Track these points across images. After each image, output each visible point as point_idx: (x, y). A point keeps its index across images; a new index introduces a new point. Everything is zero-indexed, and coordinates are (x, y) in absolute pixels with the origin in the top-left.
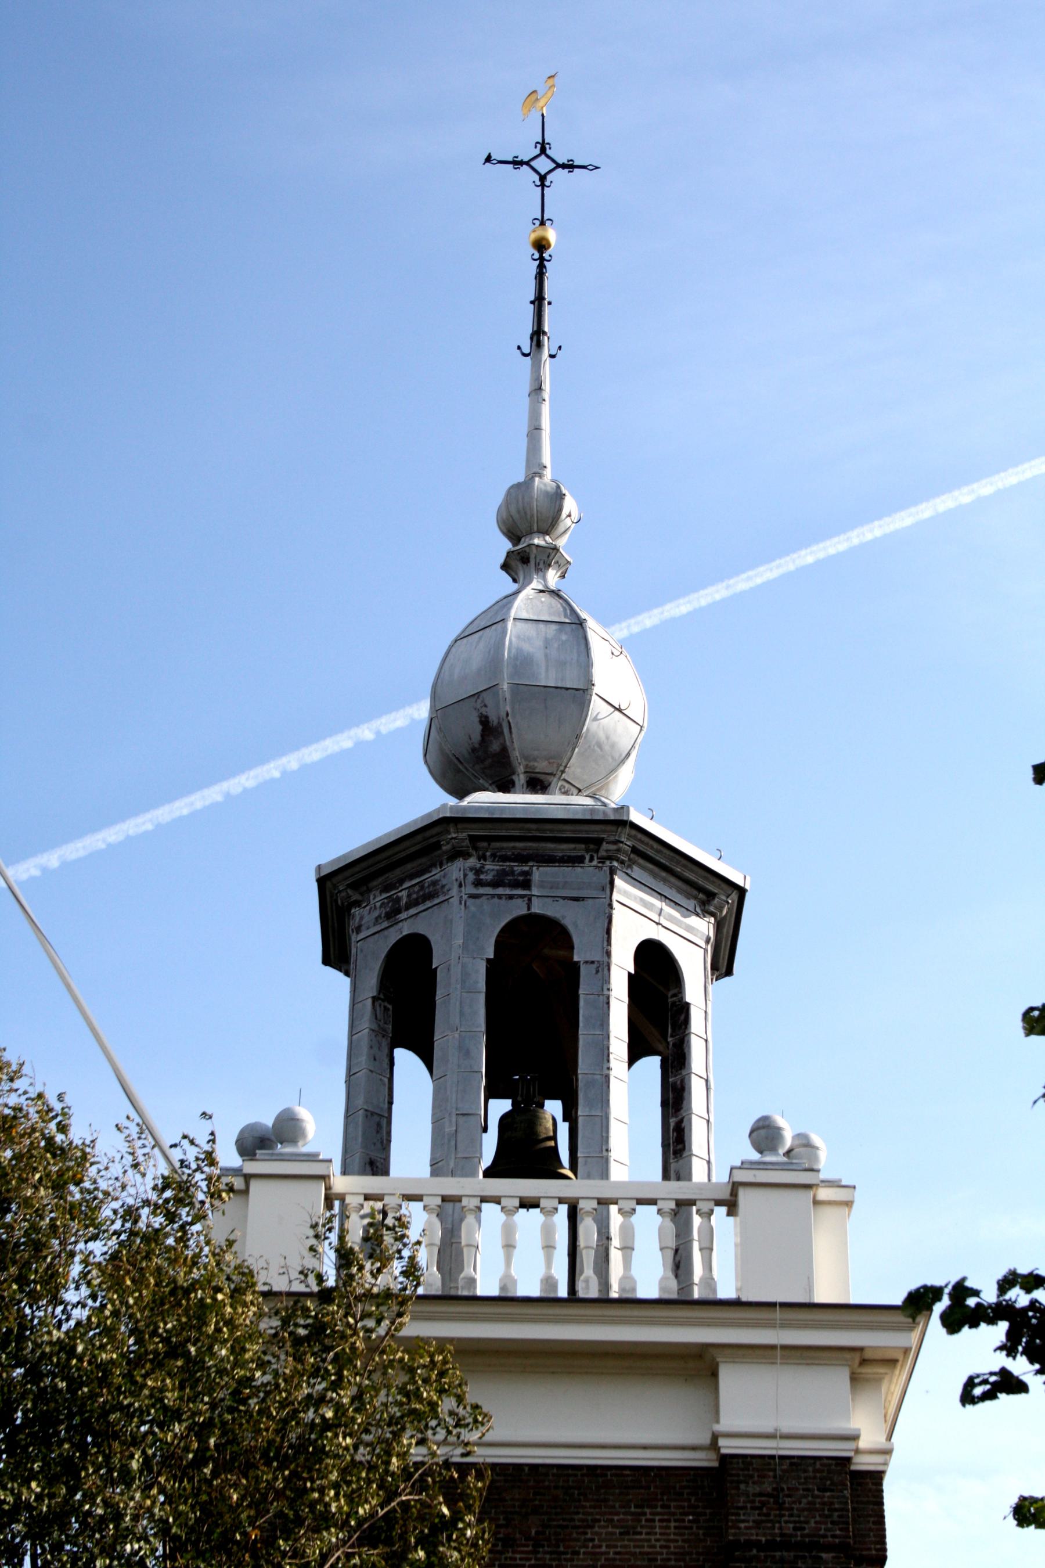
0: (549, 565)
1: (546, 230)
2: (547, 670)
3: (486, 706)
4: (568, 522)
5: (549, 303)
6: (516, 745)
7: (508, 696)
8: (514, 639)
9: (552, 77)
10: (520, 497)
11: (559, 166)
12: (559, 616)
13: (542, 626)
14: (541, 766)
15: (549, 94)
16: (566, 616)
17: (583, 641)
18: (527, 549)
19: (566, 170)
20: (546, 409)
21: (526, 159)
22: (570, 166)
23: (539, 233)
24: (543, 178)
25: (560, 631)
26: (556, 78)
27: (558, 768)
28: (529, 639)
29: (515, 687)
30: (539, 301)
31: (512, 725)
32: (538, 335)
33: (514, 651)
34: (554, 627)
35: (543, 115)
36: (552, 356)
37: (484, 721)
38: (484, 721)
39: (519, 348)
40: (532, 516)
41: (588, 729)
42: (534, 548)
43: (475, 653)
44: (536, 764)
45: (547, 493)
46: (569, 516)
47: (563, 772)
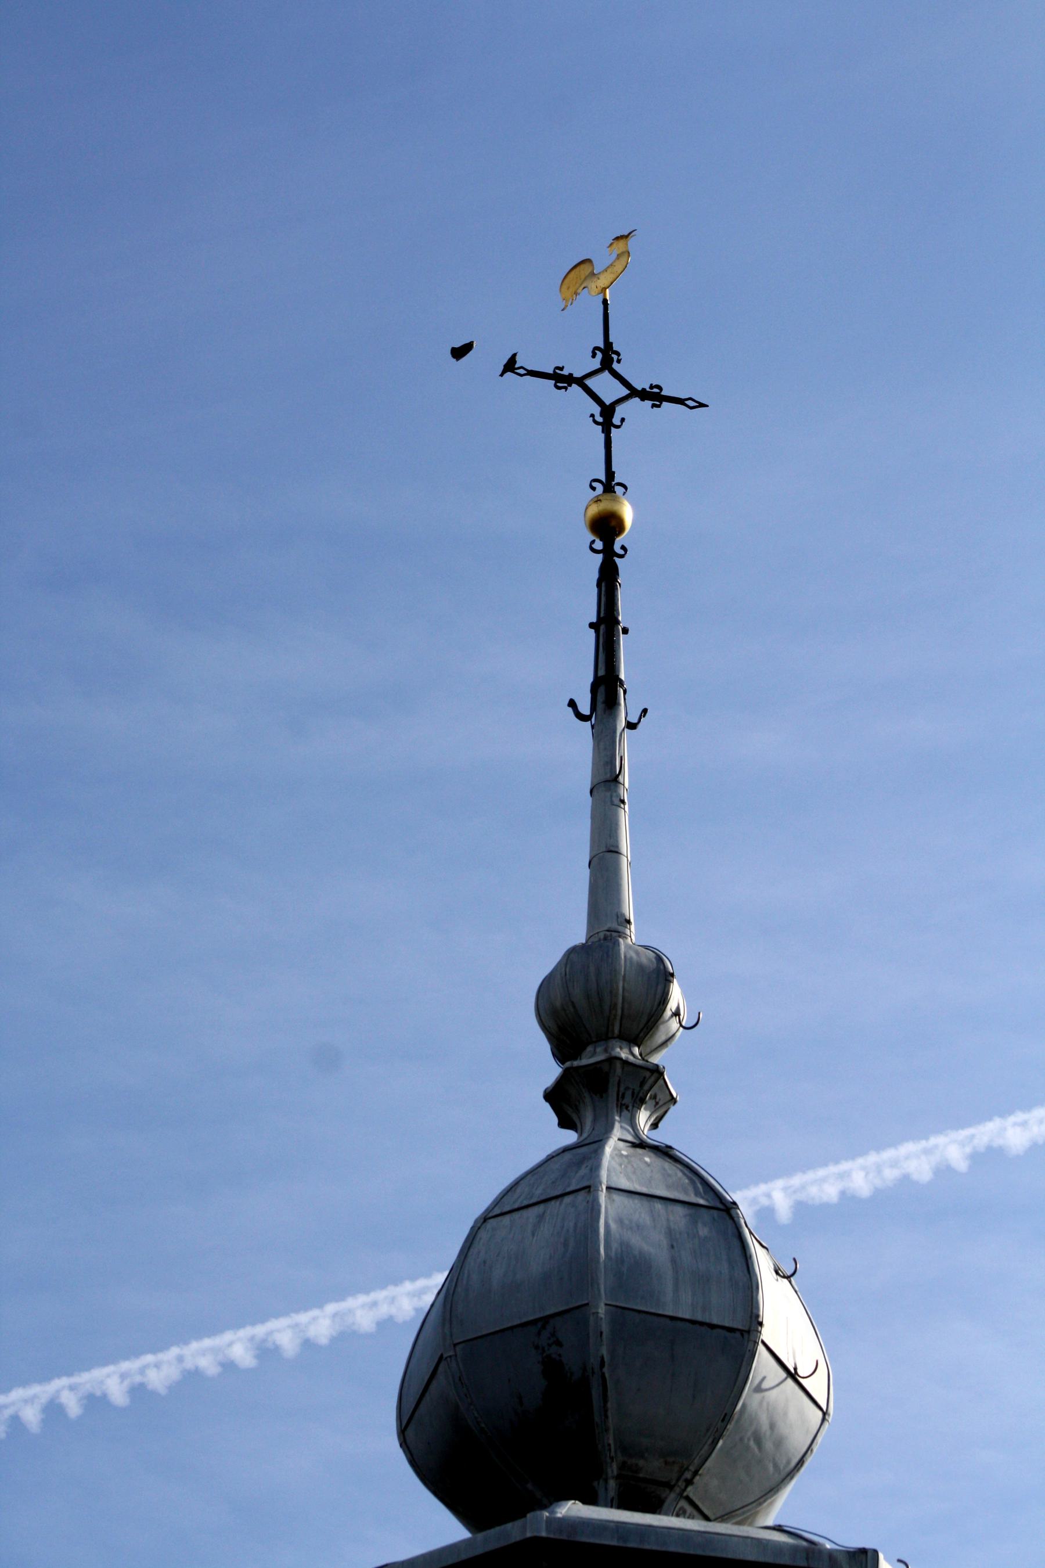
0: (642, 1101)
1: (616, 500)
2: (676, 1289)
3: (559, 1344)
4: (674, 1024)
5: (625, 631)
6: (611, 1423)
7: (605, 1328)
8: (613, 1226)
9: (627, 237)
10: (592, 969)
11: (634, 393)
12: (686, 1193)
13: (658, 1206)
14: (652, 1467)
15: (619, 267)
16: (697, 1193)
17: (736, 1242)
18: (606, 1067)
19: (648, 403)
20: (624, 818)
21: (577, 374)
22: (655, 396)
23: (605, 506)
24: (608, 411)
25: (694, 1221)
26: (631, 241)
27: (681, 1473)
28: (639, 1228)
29: (619, 1312)
30: (607, 626)
31: (610, 1385)
32: (607, 686)
33: (615, 1246)
34: (680, 1210)
35: (605, 302)
36: (631, 726)
37: (552, 1367)
38: (552, 1367)
39: (572, 704)
40: (613, 1007)
41: (744, 1406)
42: (618, 1065)
43: (538, 1243)
44: (641, 1463)
45: (641, 967)
46: (677, 1014)
47: (689, 1482)
